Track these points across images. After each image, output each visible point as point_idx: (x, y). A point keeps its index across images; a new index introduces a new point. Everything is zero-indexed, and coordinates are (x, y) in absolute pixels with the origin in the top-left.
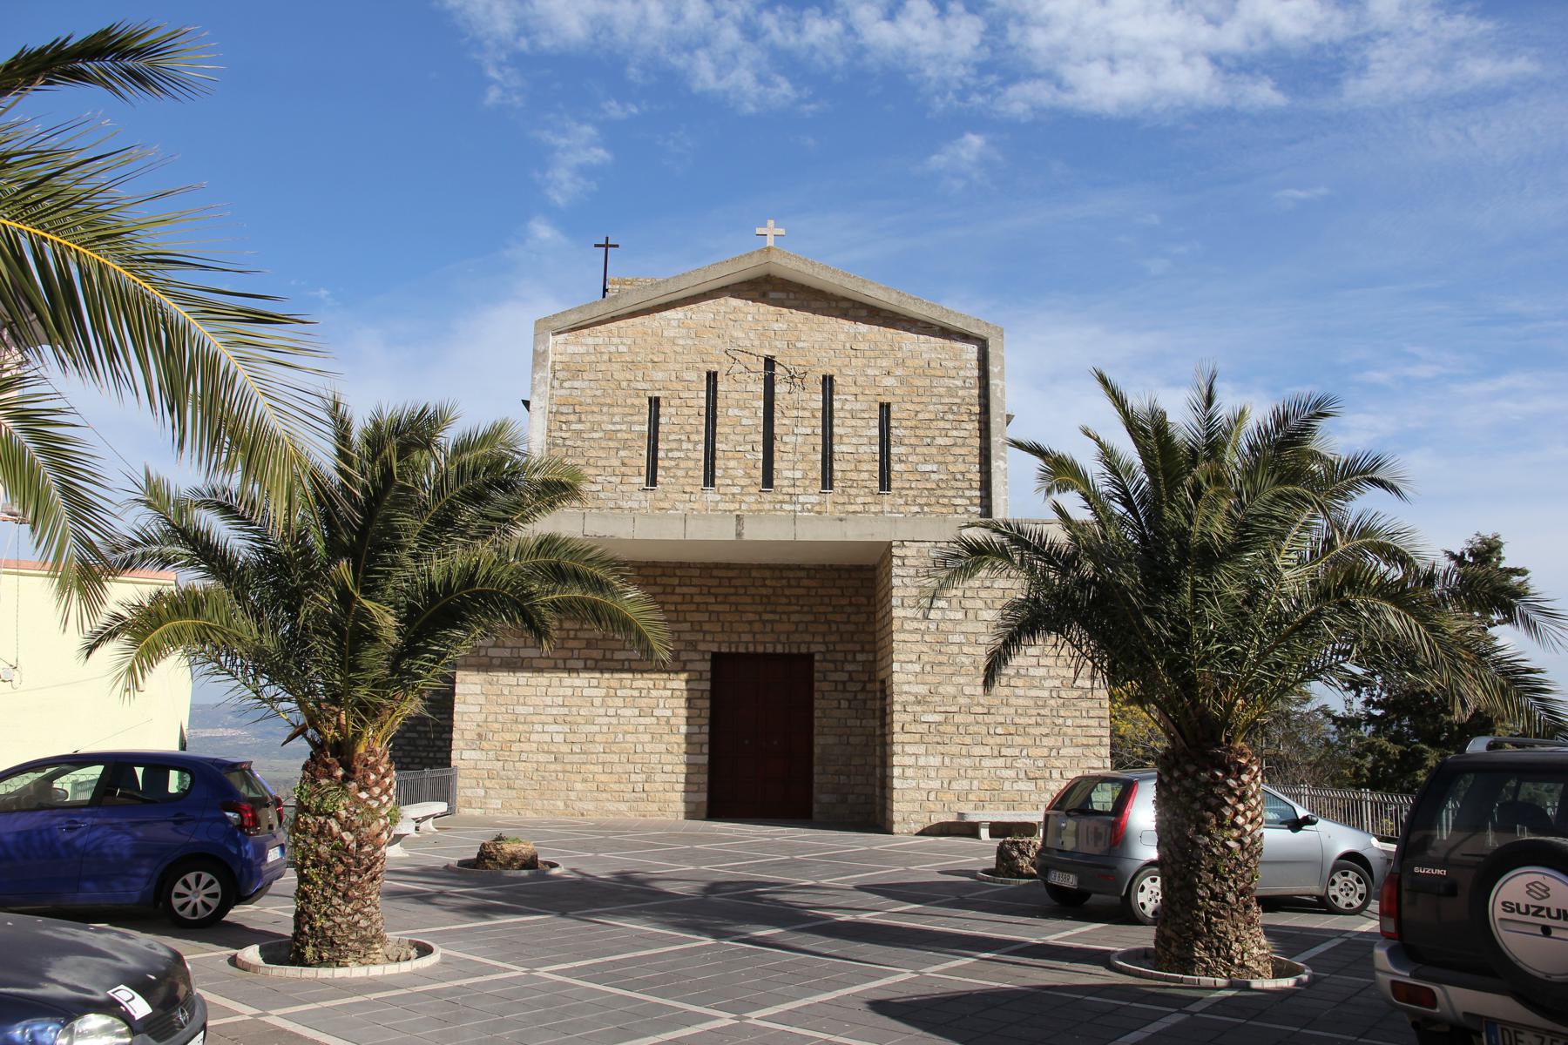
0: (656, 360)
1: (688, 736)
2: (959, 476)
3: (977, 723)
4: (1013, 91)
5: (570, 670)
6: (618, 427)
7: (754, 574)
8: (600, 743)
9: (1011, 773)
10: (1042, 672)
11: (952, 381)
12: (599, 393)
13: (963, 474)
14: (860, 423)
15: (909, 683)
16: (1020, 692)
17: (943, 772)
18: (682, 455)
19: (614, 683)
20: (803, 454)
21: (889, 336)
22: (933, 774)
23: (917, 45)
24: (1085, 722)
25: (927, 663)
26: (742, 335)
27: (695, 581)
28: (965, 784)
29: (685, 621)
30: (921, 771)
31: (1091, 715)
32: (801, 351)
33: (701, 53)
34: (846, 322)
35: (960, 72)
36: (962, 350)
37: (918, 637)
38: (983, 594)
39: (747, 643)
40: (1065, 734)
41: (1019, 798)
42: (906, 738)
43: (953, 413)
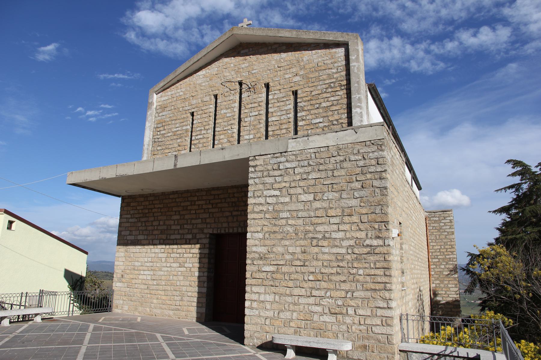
0: (193, 95)
1: (199, 277)
2: (335, 122)
3: (297, 272)
4: (526, 47)
5: (154, 245)
6: (178, 129)
7: (229, 191)
8: (164, 280)
9: (319, 309)
10: (341, 235)
11: (330, 71)
12: (171, 115)
13: (337, 120)
14: (282, 104)
15: (256, 245)
16: (326, 250)
17: (275, 306)
18: (201, 136)
19: (170, 251)
20: (254, 126)
21: (297, 55)
22: (268, 307)
23: (485, 42)
24: (373, 272)
25: (267, 232)
26: (228, 74)
27: (204, 198)
28: (288, 315)
29: (199, 218)
30: (261, 304)
31: (377, 266)
32: (254, 75)
33: (412, 61)
34: (275, 55)
35: (505, 45)
36: (335, 52)
37: (262, 215)
38: (302, 184)
39: (225, 228)
40: (358, 281)
41: (324, 327)
42: (254, 281)
43: (331, 88)
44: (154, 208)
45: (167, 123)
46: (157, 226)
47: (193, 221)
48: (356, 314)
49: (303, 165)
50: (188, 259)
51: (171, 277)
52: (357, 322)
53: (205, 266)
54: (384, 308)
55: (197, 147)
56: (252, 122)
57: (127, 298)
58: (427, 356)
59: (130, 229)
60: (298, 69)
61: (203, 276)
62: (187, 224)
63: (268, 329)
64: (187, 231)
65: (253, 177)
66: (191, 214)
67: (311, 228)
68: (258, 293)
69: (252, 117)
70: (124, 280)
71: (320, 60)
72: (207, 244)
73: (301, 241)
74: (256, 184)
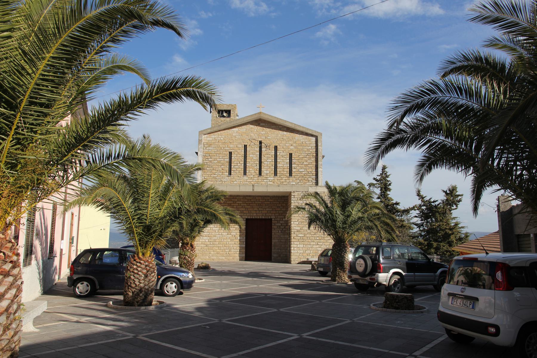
2: (310, 172)
7: (257, 198)
12: (216, 151)
13: (311, 172)
14: (284, 158)
20: (269, 167)
22: (301, 249)
28: (309, 252)
42: (295, 240)
43: (309, 156)
45: (213, 155)
50: (233, 231)
60: (293, 142)
63: (301, 257)
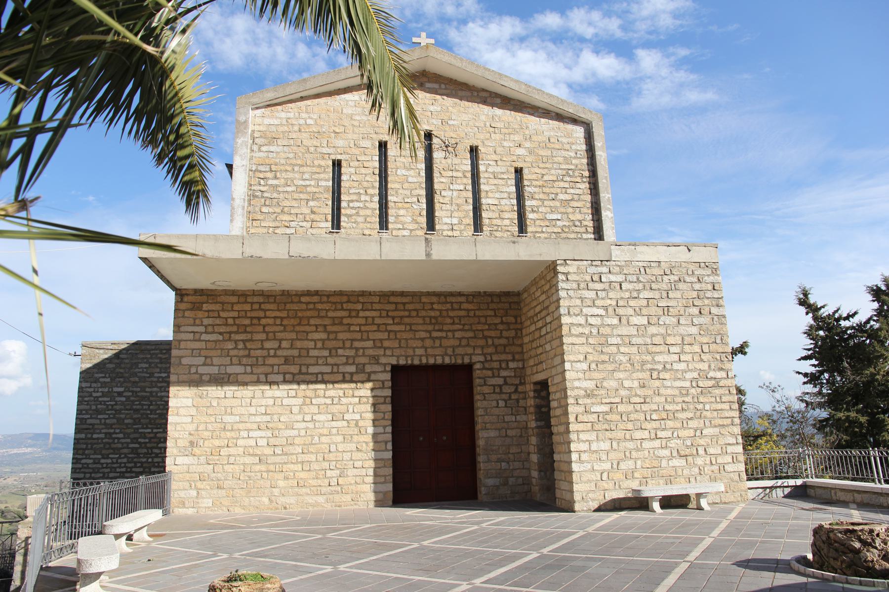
1: (375, 435)
2: (577, 223)
3: (637, 411)
5: (271, 383)
7: (424, 299)
9: (666, 452)
10: (682, 366)
13: (580, 221)
15: (579, 379)
19: (309, 393)
21: (519, 119)
24: (719, 406)
27: (376, 306)
29: (368, 339)
31: (723, 400)
34: (485, 107)
37: (583, 340)
39: (421, 356)
42: (580, 427)
44: (265, 317)
46: (275, 349)
47: (357, 344)
48: (707, 454)
49: (631, 280)
51: (316, 438)
52: (708, 462)
53: (386, 418)
54: (733, 444)
55: (353, 221)
56: (456, 200)
57: (209, 485)
58: (761, 490)
59: (203, 353)
61: (384, 433)
62: (344, 348)
64: (344, 360)
65: (566, 288)
66: (350, 331)
67: (649, 358)
68: (587, 441)
69: (454, 192)
70: (197, 451)
71: (552, 134)
72: (388, 380)
73: (639, 373)
74: (571, 297)
